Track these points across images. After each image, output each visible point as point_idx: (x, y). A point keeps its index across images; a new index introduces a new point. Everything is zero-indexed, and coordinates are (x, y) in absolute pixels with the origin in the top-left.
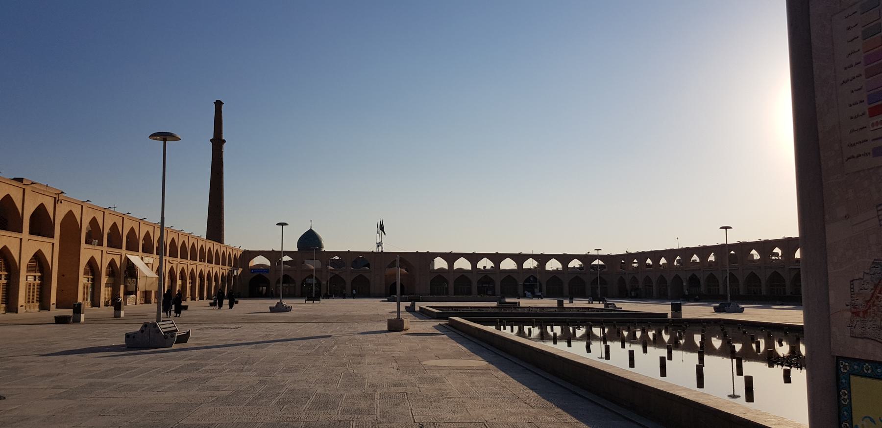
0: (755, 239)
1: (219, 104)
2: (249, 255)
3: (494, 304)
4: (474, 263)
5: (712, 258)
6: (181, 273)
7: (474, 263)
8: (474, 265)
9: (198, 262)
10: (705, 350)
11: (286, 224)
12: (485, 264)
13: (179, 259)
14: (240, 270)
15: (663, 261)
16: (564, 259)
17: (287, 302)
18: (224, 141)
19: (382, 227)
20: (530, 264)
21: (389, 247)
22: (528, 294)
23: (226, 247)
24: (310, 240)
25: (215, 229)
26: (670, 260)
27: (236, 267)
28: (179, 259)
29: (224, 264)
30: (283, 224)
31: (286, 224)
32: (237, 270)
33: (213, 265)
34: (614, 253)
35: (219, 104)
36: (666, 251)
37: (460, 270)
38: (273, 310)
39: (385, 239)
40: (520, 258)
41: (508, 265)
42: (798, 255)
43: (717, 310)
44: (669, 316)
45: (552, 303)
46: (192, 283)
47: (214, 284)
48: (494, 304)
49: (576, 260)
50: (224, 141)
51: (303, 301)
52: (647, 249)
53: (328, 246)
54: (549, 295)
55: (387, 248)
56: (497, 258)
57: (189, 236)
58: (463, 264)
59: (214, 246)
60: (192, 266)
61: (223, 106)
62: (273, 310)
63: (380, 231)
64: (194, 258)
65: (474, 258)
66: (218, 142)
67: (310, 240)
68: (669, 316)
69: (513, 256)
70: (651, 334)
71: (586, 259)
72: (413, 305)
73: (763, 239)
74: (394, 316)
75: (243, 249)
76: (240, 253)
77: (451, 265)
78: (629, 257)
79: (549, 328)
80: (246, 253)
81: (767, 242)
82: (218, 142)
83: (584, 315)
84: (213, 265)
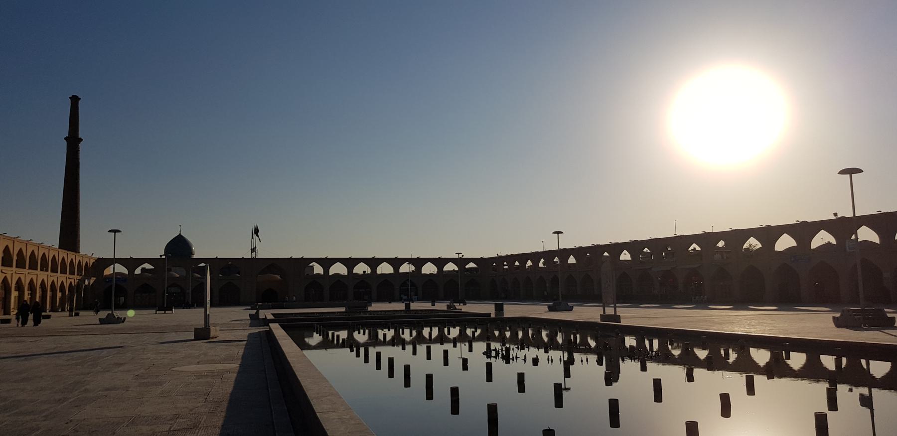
0: (646, 238)
1: (75, 100)
2: (102, 263)
3: (343, 309)
4: (350, 268)
5: (572, 260)
6: (29, 284)
7: (350, 268)
8: (350, 270)
9: (38, 272)
10: (570, 348)
11: (119, 231)
12: (361, 269)
13: (14, 268)
14: (93, 280)
15: (529, 263)
16: (440, 262)
17: (118, 313)
18: (81, 140)
19: (256, 231)
20: (405, 268)
21: (264, 253)
22: (415, 297)
23: (83, 257)
24: (179, 247)
25: (70, 235)
26: (536, 261)
27: (88, 275)
28: (14, 268)
29: (72, 273)
30: (115, 231)
31: (119, 231)
32: (89, 279)
33: (59, 274)
34: (487, 255)
35: (75, 100)
36: (532, 254)
37: (337, 275)
38: (102, 322)
39: (259, 246)
40: (396, 262)
41: (385, 269)
42: (606, 254)
43: (551, 309)
44: (493, 316)
45: (401, 306)
46: (31, 294)
47: (59, 295)
48: (343, 309)
49: (338, 263)
50: (81, 140)
51: (154, 311)
52: (504, 254)
53: (200, 251)
54: (400, 300)
55: (261, 254)
56: (373, 262)
57: (39, 246)
58: (339, 269)
59: (70, 256)
60: (18, 276)
61: (80, 102)
62: (102, 322)
63: (255, 236)
64: (54, 270)
65: (350, 263)
66: (73, 141)
67: (179, 247)
68: (493, 316)
69: (389, 261)
70: (508, 334)
71: (461, 262)
72: (257, 313)
73: (613, 242)
74: (201, 323)
75: (96, 256)
76: (92, 261)
77: (374, 269)
78: (500, 259)
79: (446, 330)
80: (99, 261)
81: (636, 242)
82: (73, 141)
83: (394, 317)
84: (59, 274)
